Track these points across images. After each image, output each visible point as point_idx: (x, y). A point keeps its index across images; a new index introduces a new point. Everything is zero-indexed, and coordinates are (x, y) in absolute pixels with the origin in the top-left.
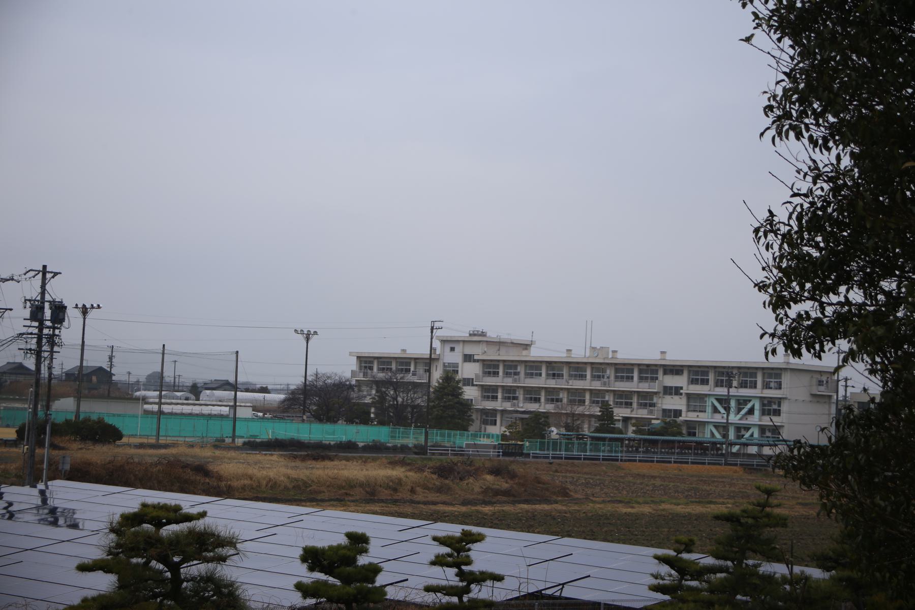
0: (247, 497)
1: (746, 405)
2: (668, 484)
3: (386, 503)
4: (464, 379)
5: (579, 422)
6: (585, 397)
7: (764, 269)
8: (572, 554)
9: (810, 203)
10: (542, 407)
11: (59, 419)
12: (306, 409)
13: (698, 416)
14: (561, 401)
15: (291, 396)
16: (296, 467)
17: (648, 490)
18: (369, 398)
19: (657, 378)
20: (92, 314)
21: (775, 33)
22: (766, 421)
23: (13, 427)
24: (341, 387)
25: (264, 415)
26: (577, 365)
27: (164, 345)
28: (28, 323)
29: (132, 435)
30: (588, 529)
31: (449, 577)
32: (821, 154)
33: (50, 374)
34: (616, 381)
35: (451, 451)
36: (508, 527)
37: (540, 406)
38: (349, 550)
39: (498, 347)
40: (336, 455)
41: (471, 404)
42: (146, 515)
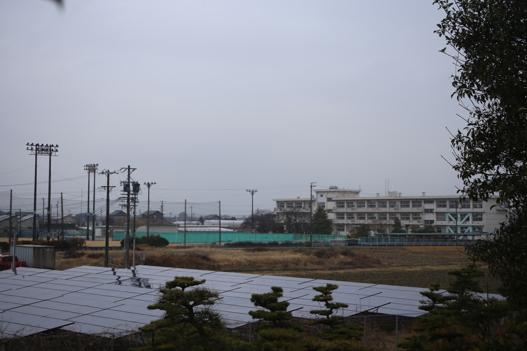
0: (227, 270)
1: (465, 216)
2: (428, 256)
4: (328, 210)
5: (384, 228)
6: (386, 216)
7: (457, 159)
8: (382, 292)
9: (477, 128)
10: (366, 222)
11: (140, 236)
12: (254, 227)
13: (442, 223)
15: (246, 221)
16: (250, 255)
17: (419, 259)
18: (283, 220)
19: (421, 205)
20: (152, 187)
21: (456, 47)
22: (476, 223)
23: (119, 241)
24: (269, 217)
25: (234, 230)
26: (382, 201)
27: (186, 200)
28: (123, 193)
29: (173, 242)
30: (390, 279)
31: (321, 306)
32: (481, 104)
33: (135, 215)
34: (401, 208)
37: (365, 221)
38: (273, 295)
40: (268, 249)
41: (332, 222)
42: (177, 282)
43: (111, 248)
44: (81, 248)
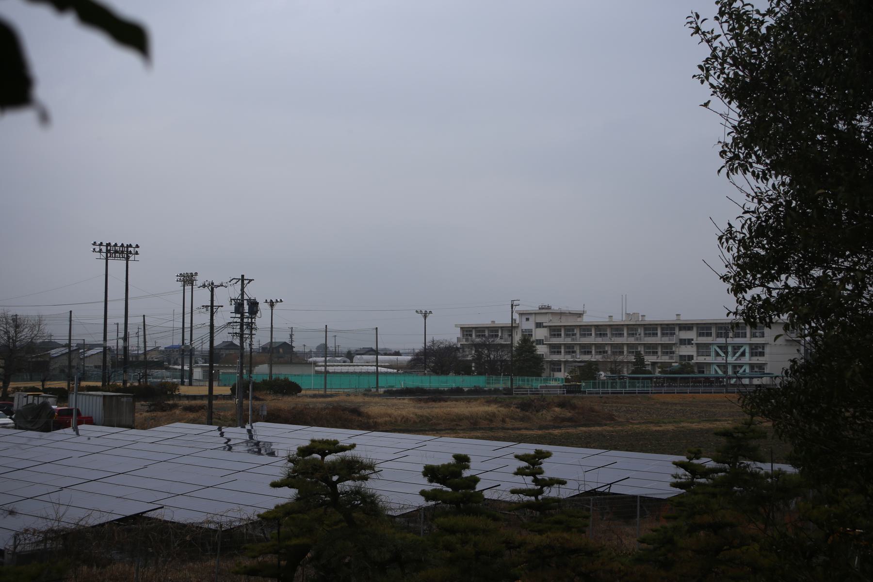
0: (388, 429)
1: (739, 349)
3: (484, 430)
4: (537, 340)
5: (620, 367)
6: (623, 349)
7: (726, 266)
10: (593, 358)
11: (259, 380)
13: (705, 359)
14: (607, 353)
19: (674, 334)
20: (277, 306)
23: (229, 386)
24: (450, 350)
26: (616, 327)
27: (326, 326)
28: (234, 315)
29: (308, 389)
31: (527, 483)
33: (251, 349)
35: (530, 391)
36: (572, 444)
37: (592, 357)
39: (560, 316)
42: (314, 448)
43: (217, 397)
44: (172, 396)
